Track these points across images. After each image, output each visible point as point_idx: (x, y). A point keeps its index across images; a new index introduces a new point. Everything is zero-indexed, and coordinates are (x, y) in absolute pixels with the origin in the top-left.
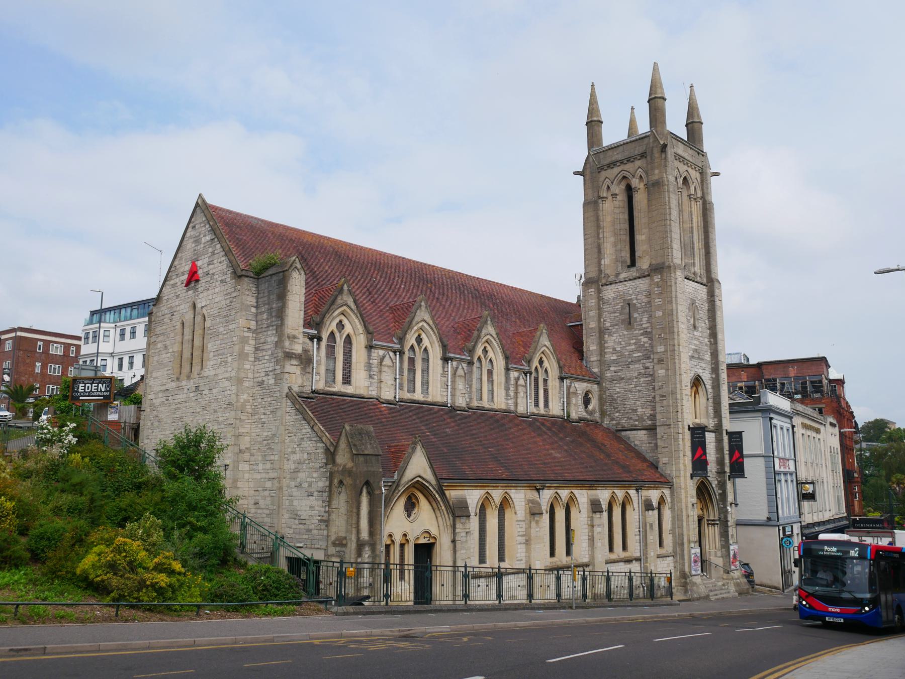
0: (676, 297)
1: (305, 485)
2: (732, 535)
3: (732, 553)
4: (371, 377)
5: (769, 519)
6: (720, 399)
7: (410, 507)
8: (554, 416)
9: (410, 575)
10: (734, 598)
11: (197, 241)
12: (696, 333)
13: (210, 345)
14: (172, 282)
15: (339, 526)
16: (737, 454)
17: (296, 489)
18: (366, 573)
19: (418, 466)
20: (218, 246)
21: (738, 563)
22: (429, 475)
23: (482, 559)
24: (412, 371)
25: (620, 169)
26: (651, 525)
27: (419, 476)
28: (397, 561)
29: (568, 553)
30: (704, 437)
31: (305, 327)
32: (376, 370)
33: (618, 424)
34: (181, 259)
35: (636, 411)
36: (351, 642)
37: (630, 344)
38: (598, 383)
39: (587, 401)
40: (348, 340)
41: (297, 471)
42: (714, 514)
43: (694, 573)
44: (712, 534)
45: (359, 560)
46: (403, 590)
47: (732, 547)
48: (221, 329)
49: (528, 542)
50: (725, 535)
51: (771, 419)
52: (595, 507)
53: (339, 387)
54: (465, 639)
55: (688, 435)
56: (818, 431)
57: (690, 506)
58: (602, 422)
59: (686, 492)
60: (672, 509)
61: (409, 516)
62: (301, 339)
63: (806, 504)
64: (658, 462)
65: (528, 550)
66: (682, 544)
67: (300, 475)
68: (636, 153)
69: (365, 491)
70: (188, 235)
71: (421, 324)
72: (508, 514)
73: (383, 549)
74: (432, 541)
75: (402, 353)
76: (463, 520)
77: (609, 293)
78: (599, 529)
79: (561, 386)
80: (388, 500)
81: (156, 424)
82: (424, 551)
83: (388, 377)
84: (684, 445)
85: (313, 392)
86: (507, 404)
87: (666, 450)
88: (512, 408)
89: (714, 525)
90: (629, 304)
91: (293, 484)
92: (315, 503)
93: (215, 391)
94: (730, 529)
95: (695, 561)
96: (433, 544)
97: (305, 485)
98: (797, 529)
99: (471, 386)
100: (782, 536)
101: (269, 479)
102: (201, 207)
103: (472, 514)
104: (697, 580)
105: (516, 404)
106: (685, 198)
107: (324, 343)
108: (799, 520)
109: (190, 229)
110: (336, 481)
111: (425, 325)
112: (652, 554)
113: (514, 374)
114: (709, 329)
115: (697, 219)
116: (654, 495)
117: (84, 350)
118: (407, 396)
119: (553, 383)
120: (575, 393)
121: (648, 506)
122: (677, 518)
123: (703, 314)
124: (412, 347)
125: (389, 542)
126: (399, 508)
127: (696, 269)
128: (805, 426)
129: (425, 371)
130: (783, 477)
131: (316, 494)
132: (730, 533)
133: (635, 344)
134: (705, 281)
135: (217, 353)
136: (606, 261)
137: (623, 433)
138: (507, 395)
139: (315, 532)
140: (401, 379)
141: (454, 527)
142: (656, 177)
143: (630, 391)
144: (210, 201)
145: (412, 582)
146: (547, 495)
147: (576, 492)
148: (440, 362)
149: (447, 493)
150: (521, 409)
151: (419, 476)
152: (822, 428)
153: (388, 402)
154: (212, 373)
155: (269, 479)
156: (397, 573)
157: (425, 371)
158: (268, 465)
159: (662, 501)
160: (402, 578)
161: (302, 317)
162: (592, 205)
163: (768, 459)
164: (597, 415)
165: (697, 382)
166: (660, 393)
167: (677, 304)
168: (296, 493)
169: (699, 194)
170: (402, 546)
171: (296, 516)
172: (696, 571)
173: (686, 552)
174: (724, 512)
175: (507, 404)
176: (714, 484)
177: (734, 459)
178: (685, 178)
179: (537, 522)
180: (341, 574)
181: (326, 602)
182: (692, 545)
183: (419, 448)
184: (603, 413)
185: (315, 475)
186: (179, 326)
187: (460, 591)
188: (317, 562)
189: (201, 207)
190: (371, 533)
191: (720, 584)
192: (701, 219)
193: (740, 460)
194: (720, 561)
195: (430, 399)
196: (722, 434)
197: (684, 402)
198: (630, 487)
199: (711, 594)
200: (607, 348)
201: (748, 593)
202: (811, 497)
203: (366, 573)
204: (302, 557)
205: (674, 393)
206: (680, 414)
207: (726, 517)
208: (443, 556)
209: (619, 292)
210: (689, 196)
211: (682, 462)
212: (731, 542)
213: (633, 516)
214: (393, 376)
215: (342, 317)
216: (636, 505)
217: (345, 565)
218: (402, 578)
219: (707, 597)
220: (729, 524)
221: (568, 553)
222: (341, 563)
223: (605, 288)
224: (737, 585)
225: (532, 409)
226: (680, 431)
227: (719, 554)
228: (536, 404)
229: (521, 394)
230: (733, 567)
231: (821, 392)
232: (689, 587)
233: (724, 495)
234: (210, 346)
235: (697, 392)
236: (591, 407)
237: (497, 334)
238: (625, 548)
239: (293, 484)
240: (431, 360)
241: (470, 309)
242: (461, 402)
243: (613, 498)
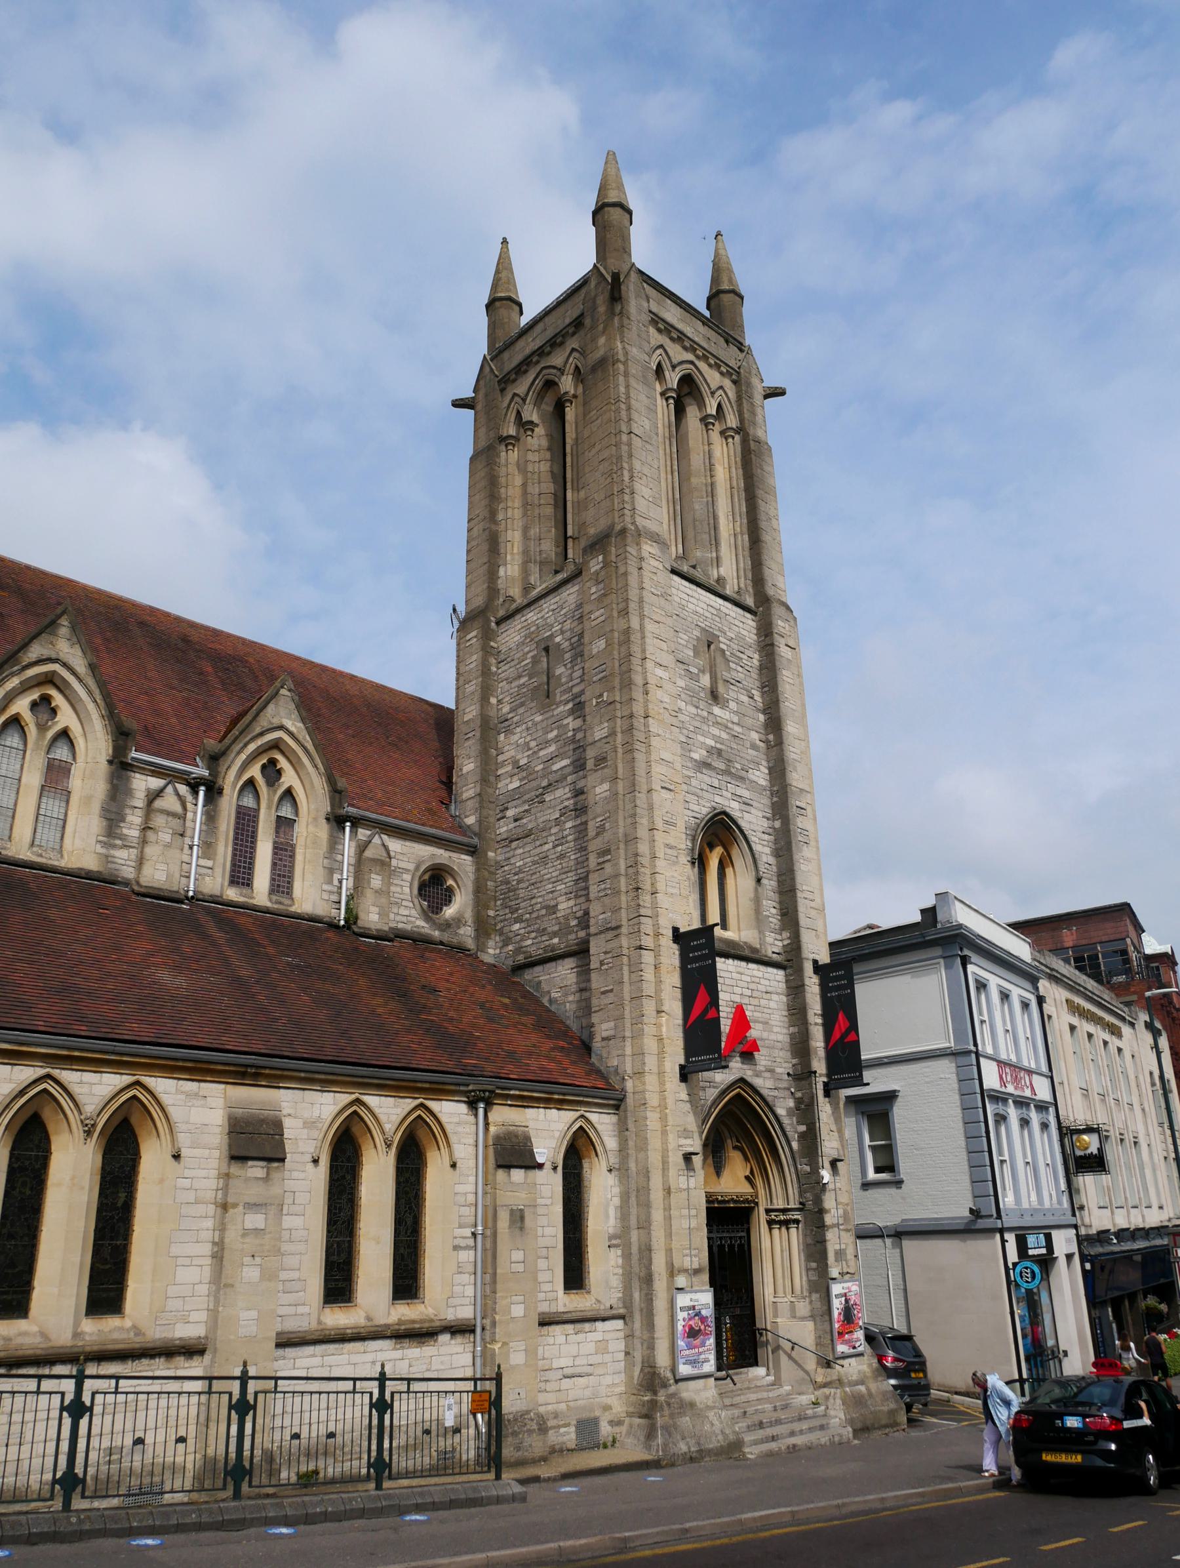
0: (641, 600)
2: (840, 1254)
3: (837, 1305)
6: (793, 879)
10: (837, 1448)
12: (717, 710)
16: (842, 1021)
21: (860, 1335)
30: (714, 963)
33: (518, 951)
35: (553, 909)
37: (548, 742)
38: (472, 851)
43: (684, 1370)
47: (836, 1289)
50: (816, 1252)
51: (965, 961)
55: (671, 955)
56: (1116, 1032)
57: (676, 1159)
58: (481, 947)
59: (663, 1119)
60: (620, 1169)
63: (1088, 1182)
64: (591, 1036)
66: (648, 1280)
68: (567, 321)
77: (511, 637)
79: (334, 845)
84: (659, 982)
87: (610, 998)
88: (128, 873)
89: (786, 1223)
90: (547, 649)
94: (831, 1235)
95: (692, 1333)
98: (1064, 1243)
100: (1013, 1256)
104: (704, 1393)
105: (141, 861)
108: (1073, 1221)
112: (516, 1309)
114: (764, 712)
116: (548, 1130)
119: (310, 830)
127: (722, 571)
128: (1073, 1008)
130: (1013, 1113)
132: (832, 1248)
136: (510, 570)
142: (600, 353)
152: (1126, 1030)
162: (485, 458)
163: (963, 1060)
165: (719, 832)
166: (596, 842)
167: (642, 617)
172: (693, 1362)
173: (660, 1304)
174: (812, 1188)
177: (837, 1035)
182: (681, 1281)
184: (483, 928)
191: (805, 1399)
193: (849, 1038)
194: (805, 1333)
196: (800, 970)
197: (661, 864)
198: (440, 1091)
199: (748, 1438)
200: (503, 764)
201: (894, 1425)
202: (1096, 1163)
205: (631, 840)
206: (646, 899)
207: (818, 1200)
209: (528, 627)
211: (649, 1030)
212: (834, 1272)
219: (733, 1448)
220: (828, 1219)
223: (503, 627)
224: (856, 1401)
225: (214, 880)
226: (648, 941)
227: (803, 1308)
230: (841, 1348)
231: (1128, 971)
232: (660, 1421)
233: (811, 1139)
237: (92, 667)
241: (182, 688)
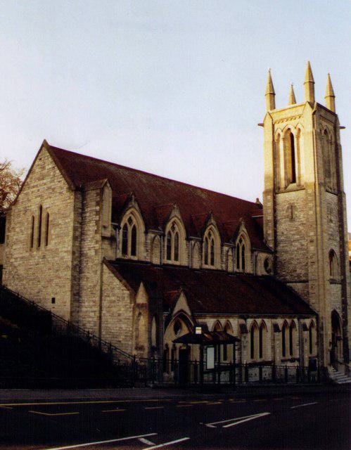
13: (52, 232)
19: (182, 304)
22: (187, 309)
29: (261, 356)
31: (112, 221)
39: (266, 264)
40: (134, 229)
52: (276, 328)
53: (129, 256)
62: (110, 228)
70: (37, 163)
72: (264, 331)
75: (164, 236)
78: (278, 342)
88: (224, 269)
101: (92, 312)
102: (45, 145)
105: (227, 267)
106: (326, 143)
107: (121, 231)
109: (38, 160)
113: (226, 248)
115: (332, 155)
116: (308, 322)
122: (320, 336)
135: (58, 236)
144: (51, 143)
146: (250, 321)
147: (266, 320)
150: (230, 269)
155: (92, 312)
158: (92, 304)
159: (312, 325)
169: (333, 141)
176: (341, 315)
178: (325, 130)
183: (182, 294)
186: (30, 219)
189: (45, 145)
210: (327, 140)
213: (296, 334)
216: (297, 328)
221: (261, 356)
228: (238, 267)
229: (230, 261)
234: (52, 232)
238: (291, 354)
243: (285, 322)
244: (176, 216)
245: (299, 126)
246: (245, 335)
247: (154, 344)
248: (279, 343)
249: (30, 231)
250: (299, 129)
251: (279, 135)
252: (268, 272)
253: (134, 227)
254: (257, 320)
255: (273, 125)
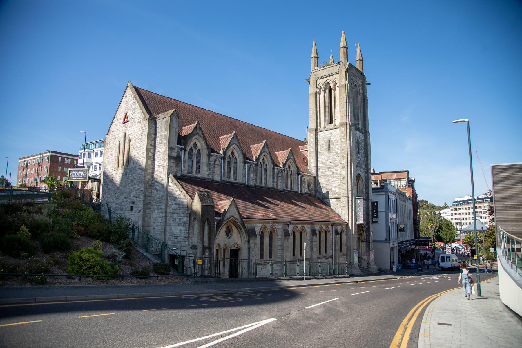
1: (177, 220)
4: (209, 170)
5: (386, 239)
7: (228, 232)
8: (294, 192)
9: (228, 264)
11: (127, 103)
14: (115, 123)
15: (196, 240)
17: (172, 222)
18: (207, 262)
20: (138, 105)
23: (262, 257)
24: (229, 168)
25: (326, 79)
26: (338, 242)
27: (233, 217)
28: (222, 257)
32: (212, 166)
33: (323, 196)
34: (120, 112)
36: (200, 297)
39: (309, 185)
40: (199, 152)
41: (173, 213)
42: (364, 236)
44: (363, 245)
45: (204, 256)
46: (225, 271)
48: (138, 145)
49: (283, 249)
50: (368, 246)
54: (258, 295)
61: (228, 236)
65: (283, 253)
67: (175, 215)
69: (206, 223)
70: (123, 100)
71: (234, 146)
72: (328, 234)
73: (215, 251)
74: (238, 248)
76: (253, 238)
78: (315, 243)
80: (218, 227)
81: (107, 191)
82: (235, 253)
83: (217, 170)
85: (181, 176)
86: (273, 185)
88: (275, 187)
91: (171, 219)
92: (182, 229)
93: (134, 175)
96: (239, 249)
97: (177, 220)
99: (256, 176)
101: (160, 217)
103: (258, 235)
105: (277, 185)
107: (187, 153)
109: (124, 97)
110: (192, 218)
111: (236, 146)
117: (80, 161)
118: (226, 179)
120: (304, 181)
121: (336, 232)
123: (362, 146)
124: (229, 156)
125: (218, 248)
126: (223, 231)
129: (235, 168)
131: (182, 224)
133: (332, 159)
134: (363, 131)
137: (325, 200)
138: (273, 181)
139: (182, 242)
140: (224, 171)
141: (249, 241)
143: (329, 181)
145: (229, 267)
148: (242, 164)
149: (246, 225)
150: (279, 187)
151: (233, 217)
153: (218, 182)
154: (133, 166)
155: (160, 217)
156: (222, 263)
157: (235, 168)
158: (160, 211)
160: (224, 265)
161: (177, 139)
164: (313, 192)
168: (173, 224)
170: (224, 250)
171: (173, 235)
174: (368, 235)
175: (273, 185)
179: (287, 240)
180: (195, 263)
181: (188, 276)
185: (182, 215)
186: (118, 143)
187: (252, 271)
188: (183, 257)
190: (210, 243)
192: (362, 104)
195: (237, 182)
203: (207, 262)
204: (175, 254)
207: (369, 238)
208: (244, 254)
214: (220, 170)
215: (196, 141)
216: (331, 233)
217: (197, 258)
218: (224, 265)
222: (195, 257)
235: (358, 182)
236: (311, 188)
239: (171, 219)
240: (238, 163)
242: (252, 183)
244: (235, 143)
245: (336, 81)
246: (287, 237)
247: (206, 244)
248: (316, 244)
249: (117, 155)
250: (336, 83)
251: (321, 88)
252: (310, 190)
253: (199, 150)
254: (305, 226)
255: (316, 81)
